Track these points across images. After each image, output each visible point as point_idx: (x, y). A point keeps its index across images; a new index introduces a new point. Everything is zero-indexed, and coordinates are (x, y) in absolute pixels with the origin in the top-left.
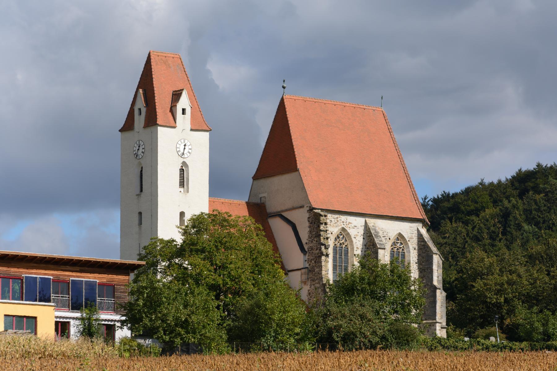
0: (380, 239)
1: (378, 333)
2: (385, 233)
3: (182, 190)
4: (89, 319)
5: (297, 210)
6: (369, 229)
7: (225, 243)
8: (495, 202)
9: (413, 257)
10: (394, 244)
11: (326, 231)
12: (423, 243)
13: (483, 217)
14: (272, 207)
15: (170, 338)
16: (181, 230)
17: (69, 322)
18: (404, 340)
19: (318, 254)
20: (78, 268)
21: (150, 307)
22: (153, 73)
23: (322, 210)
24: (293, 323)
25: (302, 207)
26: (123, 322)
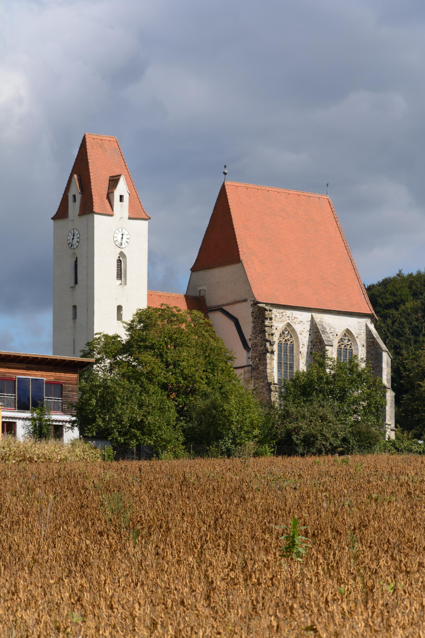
0: (328, 335)
1: (339, 435)
2: (332, 329)
3: (119, 282)
4: (40, 419)
5: (239, 304)
6: (316, 324)
7: (176, 340)
8: (415, 295)
9: (361, 353)
10: (342, 340)
11: (271, 326)
12: (371, 340)
13: (404, 311)
14: (212, 300)
15: (125, 440)
16: (126, 325)
17: (15, 423)
18: (367, 443)
19: (262, 351)
20: (25, 366)
21: (103, 407)
22: (89, 157)
23: (267, 304)
24: (252, 424)
25: (245, 301)
26: (73, 423)
